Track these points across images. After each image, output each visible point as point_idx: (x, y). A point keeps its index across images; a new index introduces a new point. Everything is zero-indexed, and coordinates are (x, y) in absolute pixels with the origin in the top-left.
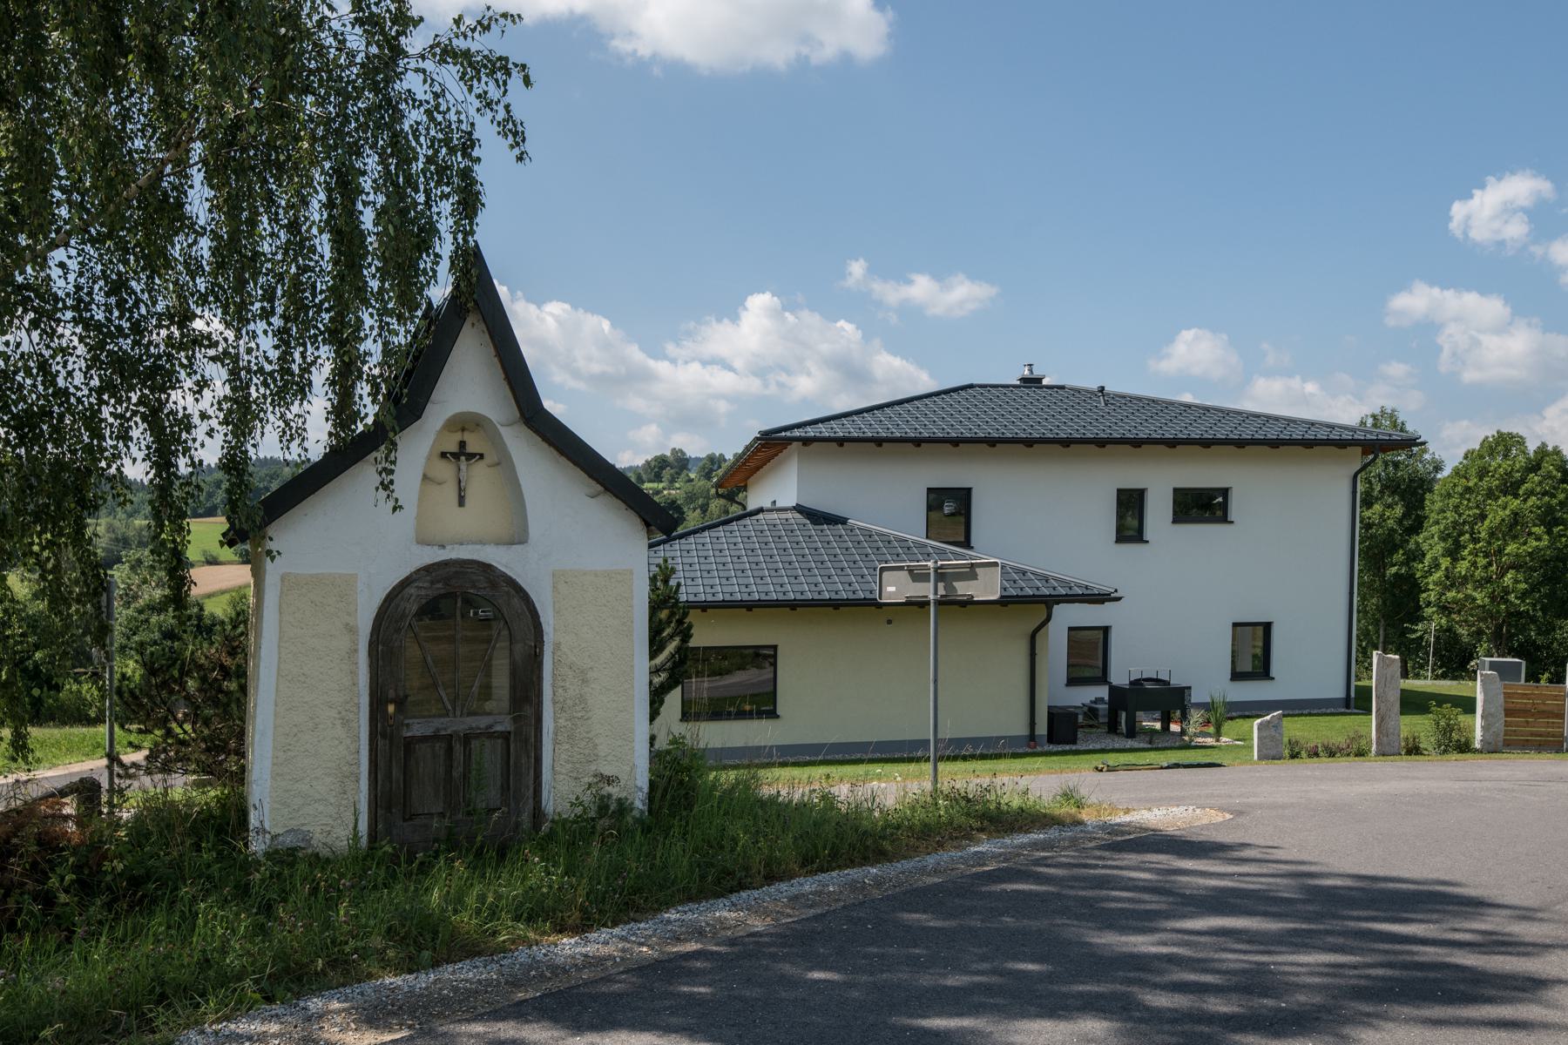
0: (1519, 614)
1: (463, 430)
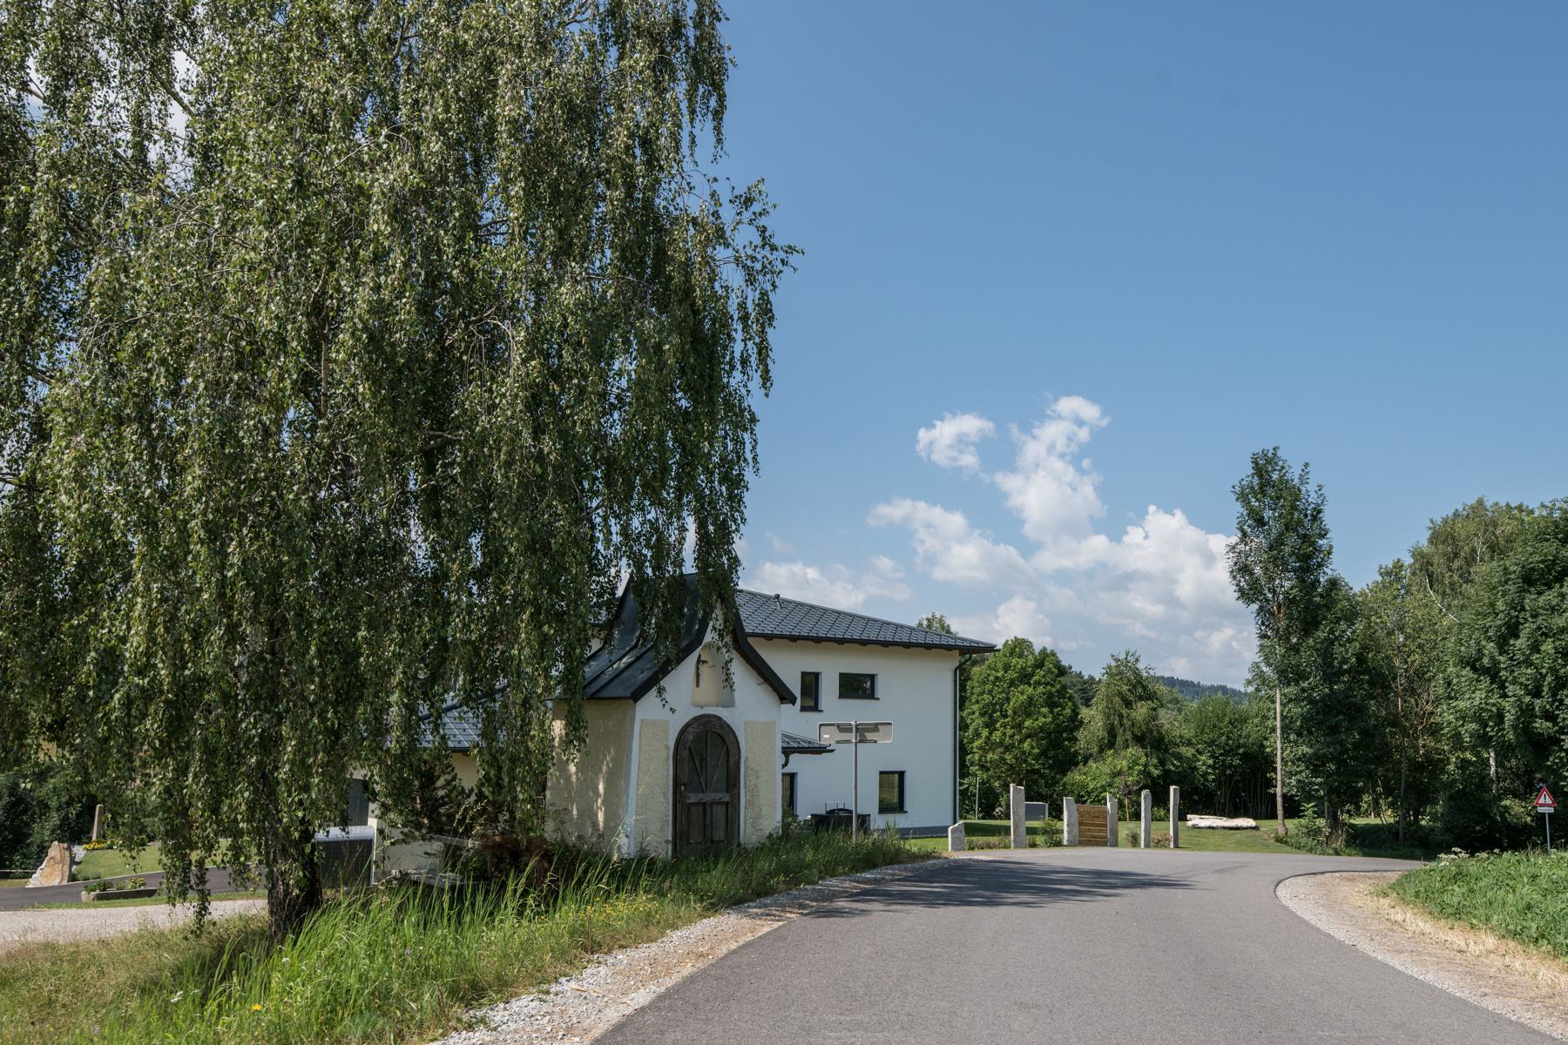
0: (1034, 771)
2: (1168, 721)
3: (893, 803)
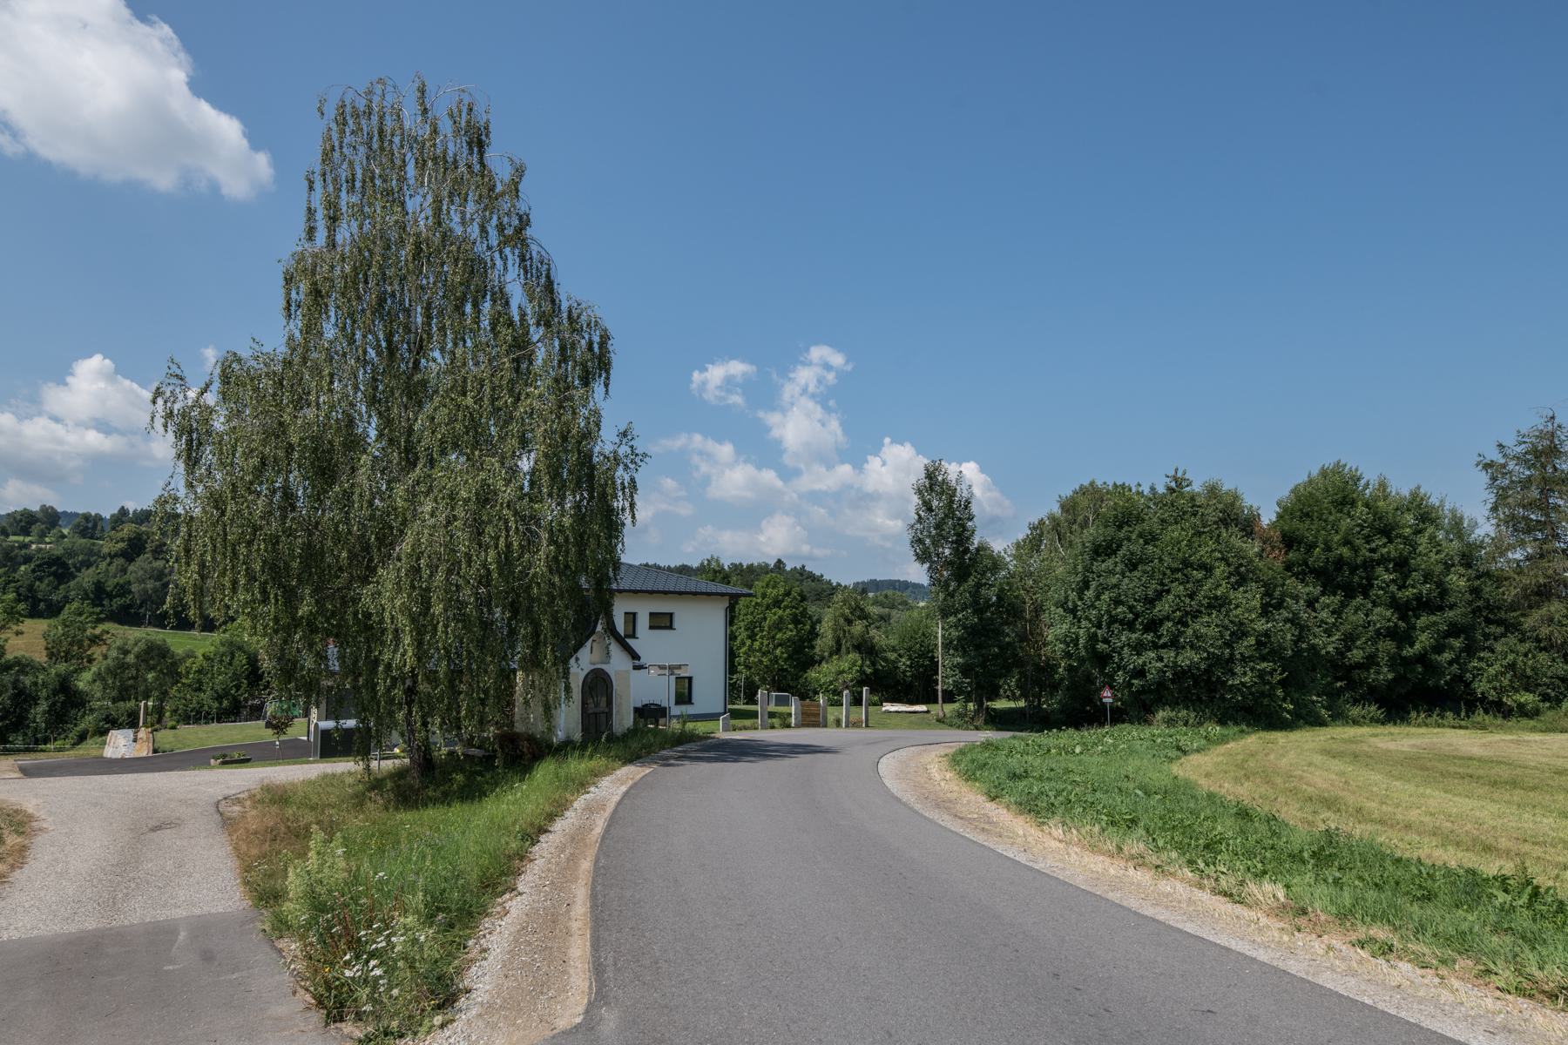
0: (783, 670)
2: (878, 636)
3: (684, 697)
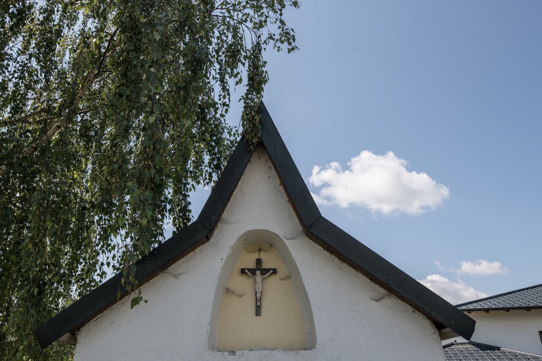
1: (260, 250)
